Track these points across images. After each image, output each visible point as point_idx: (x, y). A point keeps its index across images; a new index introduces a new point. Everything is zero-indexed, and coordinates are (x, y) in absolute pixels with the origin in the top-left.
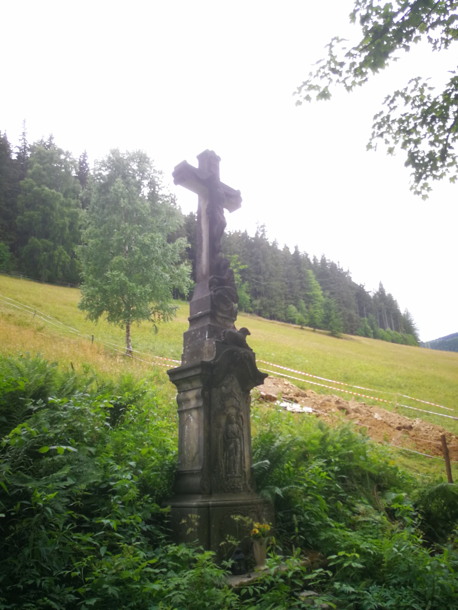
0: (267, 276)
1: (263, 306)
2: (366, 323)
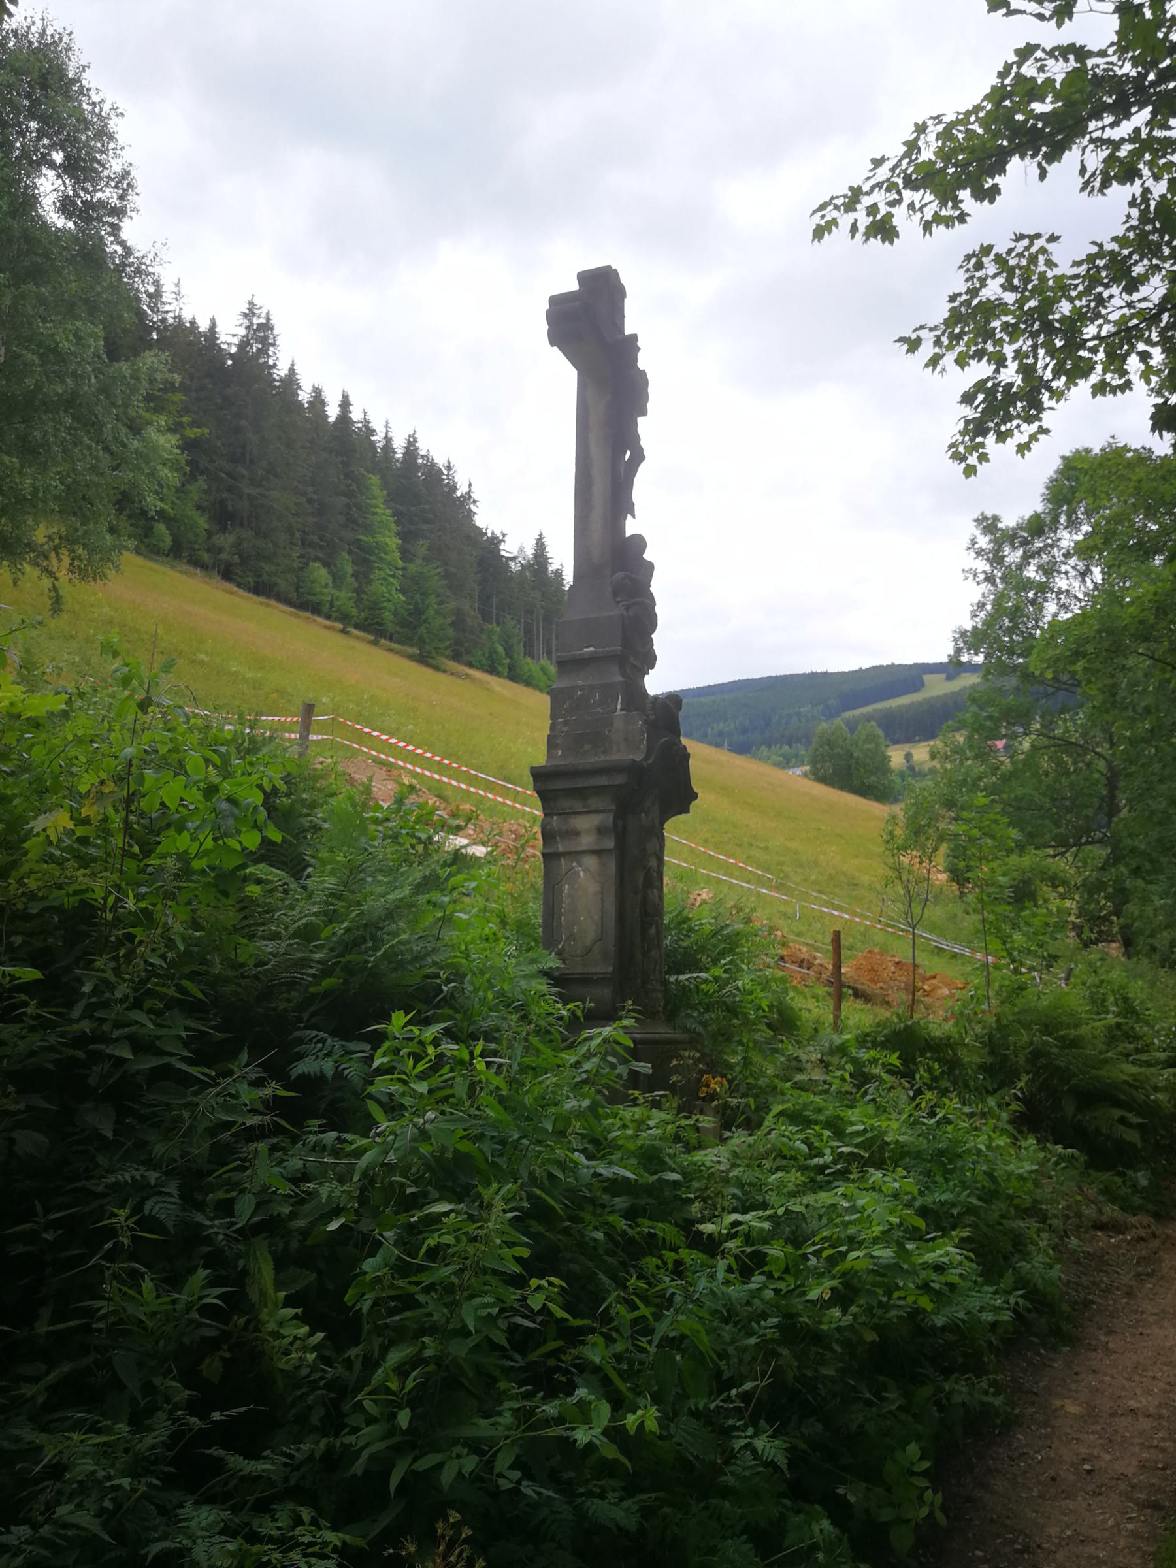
0: (260, 472)
1: (240, 556)
2: (495, 637)
